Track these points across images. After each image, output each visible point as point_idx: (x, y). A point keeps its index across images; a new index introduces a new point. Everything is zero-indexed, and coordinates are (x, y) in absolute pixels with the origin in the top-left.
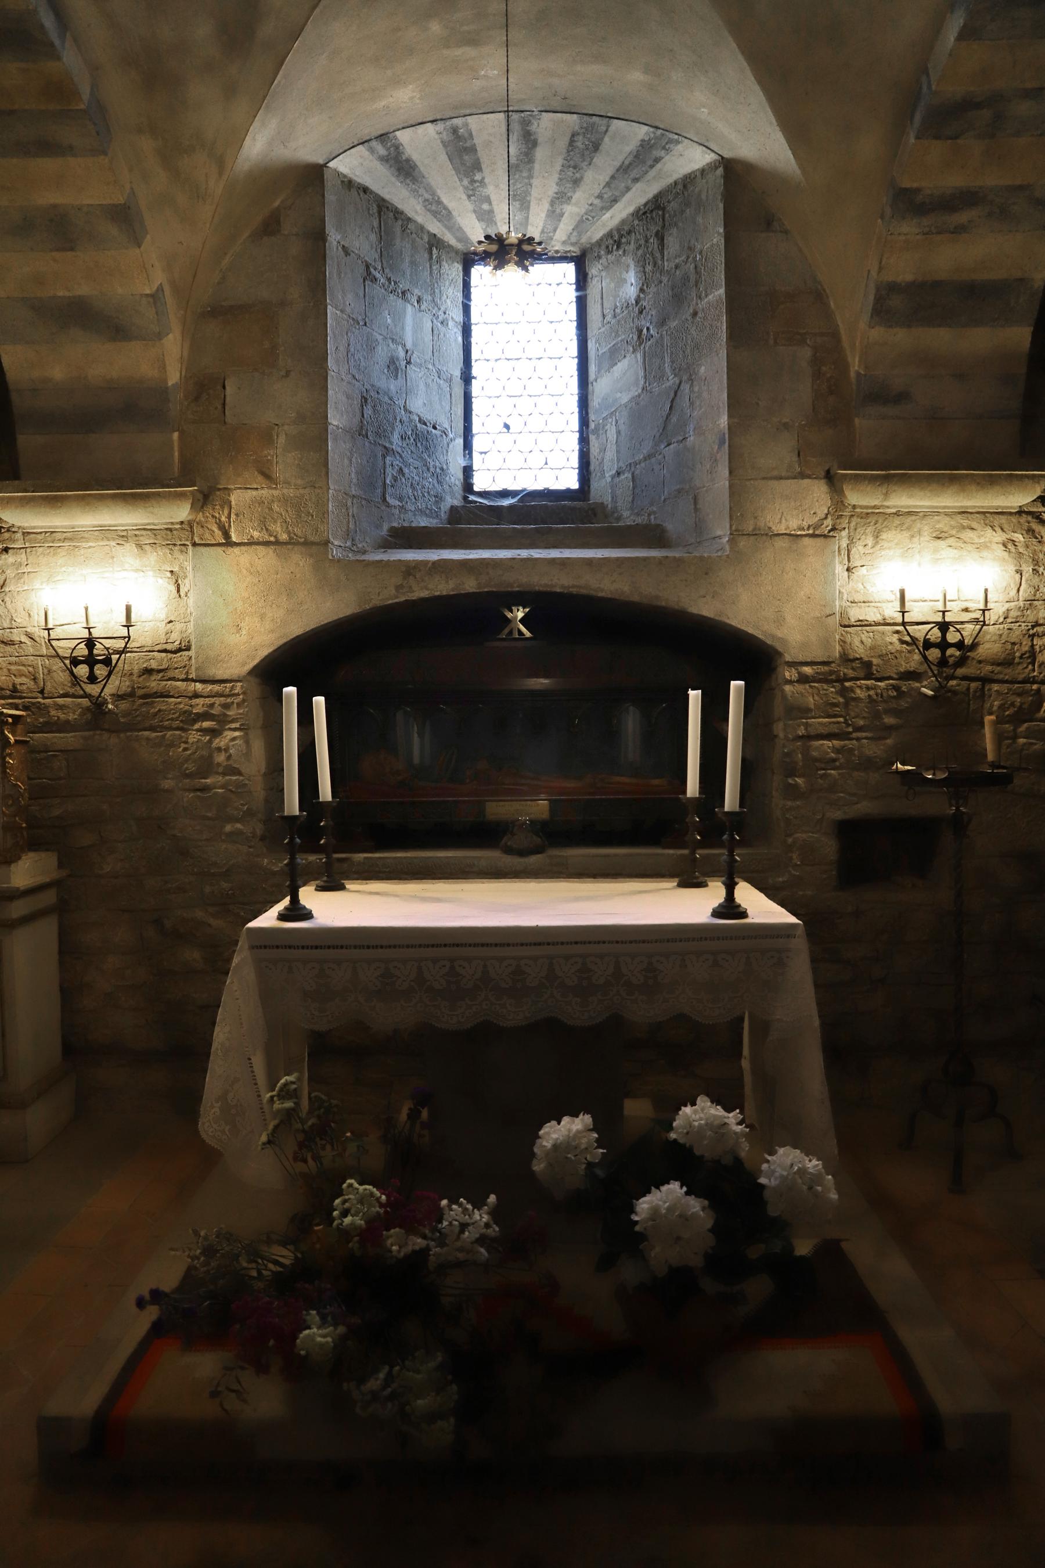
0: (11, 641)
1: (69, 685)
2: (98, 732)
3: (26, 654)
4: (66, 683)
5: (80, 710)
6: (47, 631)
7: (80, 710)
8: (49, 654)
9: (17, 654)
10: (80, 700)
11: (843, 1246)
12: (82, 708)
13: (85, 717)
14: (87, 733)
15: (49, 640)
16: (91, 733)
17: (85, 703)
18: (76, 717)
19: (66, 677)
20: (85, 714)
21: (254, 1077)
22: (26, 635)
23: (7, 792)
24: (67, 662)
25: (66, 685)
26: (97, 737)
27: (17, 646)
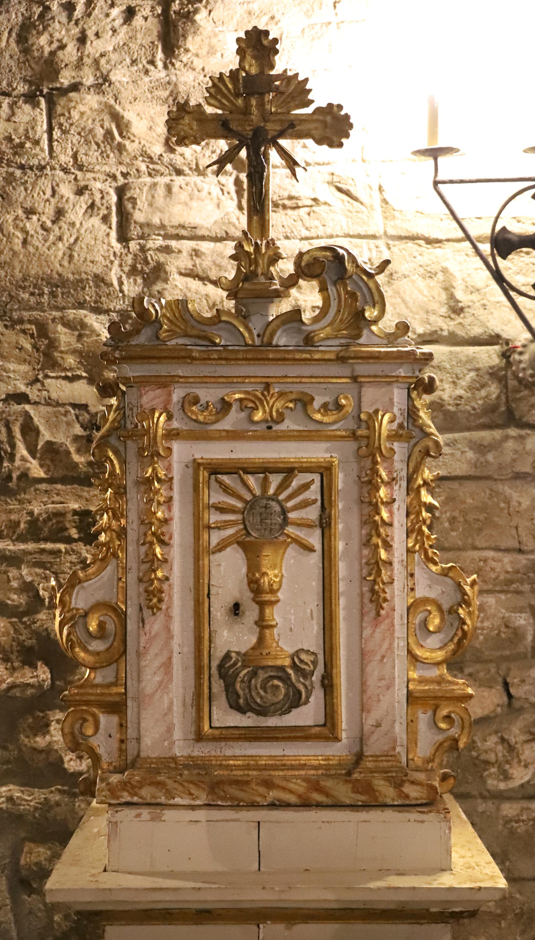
0: (290, 198)
1: (444, 310)
2: (513, 432)
3: (329, 231)
4: (434, 306)
5: (472, 374)
6: (430, 161)
7: (472, 374)
8: (391, 232)
9: (305, 233)
10: (471, 350)
11: (154, 754)
12: (478, 370)
13: (483, 393)
14: (486, 435)
15: (436, 183)
16: (497, 434)
17: (484, 356)
18: (460, 392)
19: (435, 293)
20: (483, 386)
21: (194, 888)
22: (330, 183)
23: (420, 593)
24: (486, 248)
25: (434, 313)
26: (510, 444)
27: (303, 212)
